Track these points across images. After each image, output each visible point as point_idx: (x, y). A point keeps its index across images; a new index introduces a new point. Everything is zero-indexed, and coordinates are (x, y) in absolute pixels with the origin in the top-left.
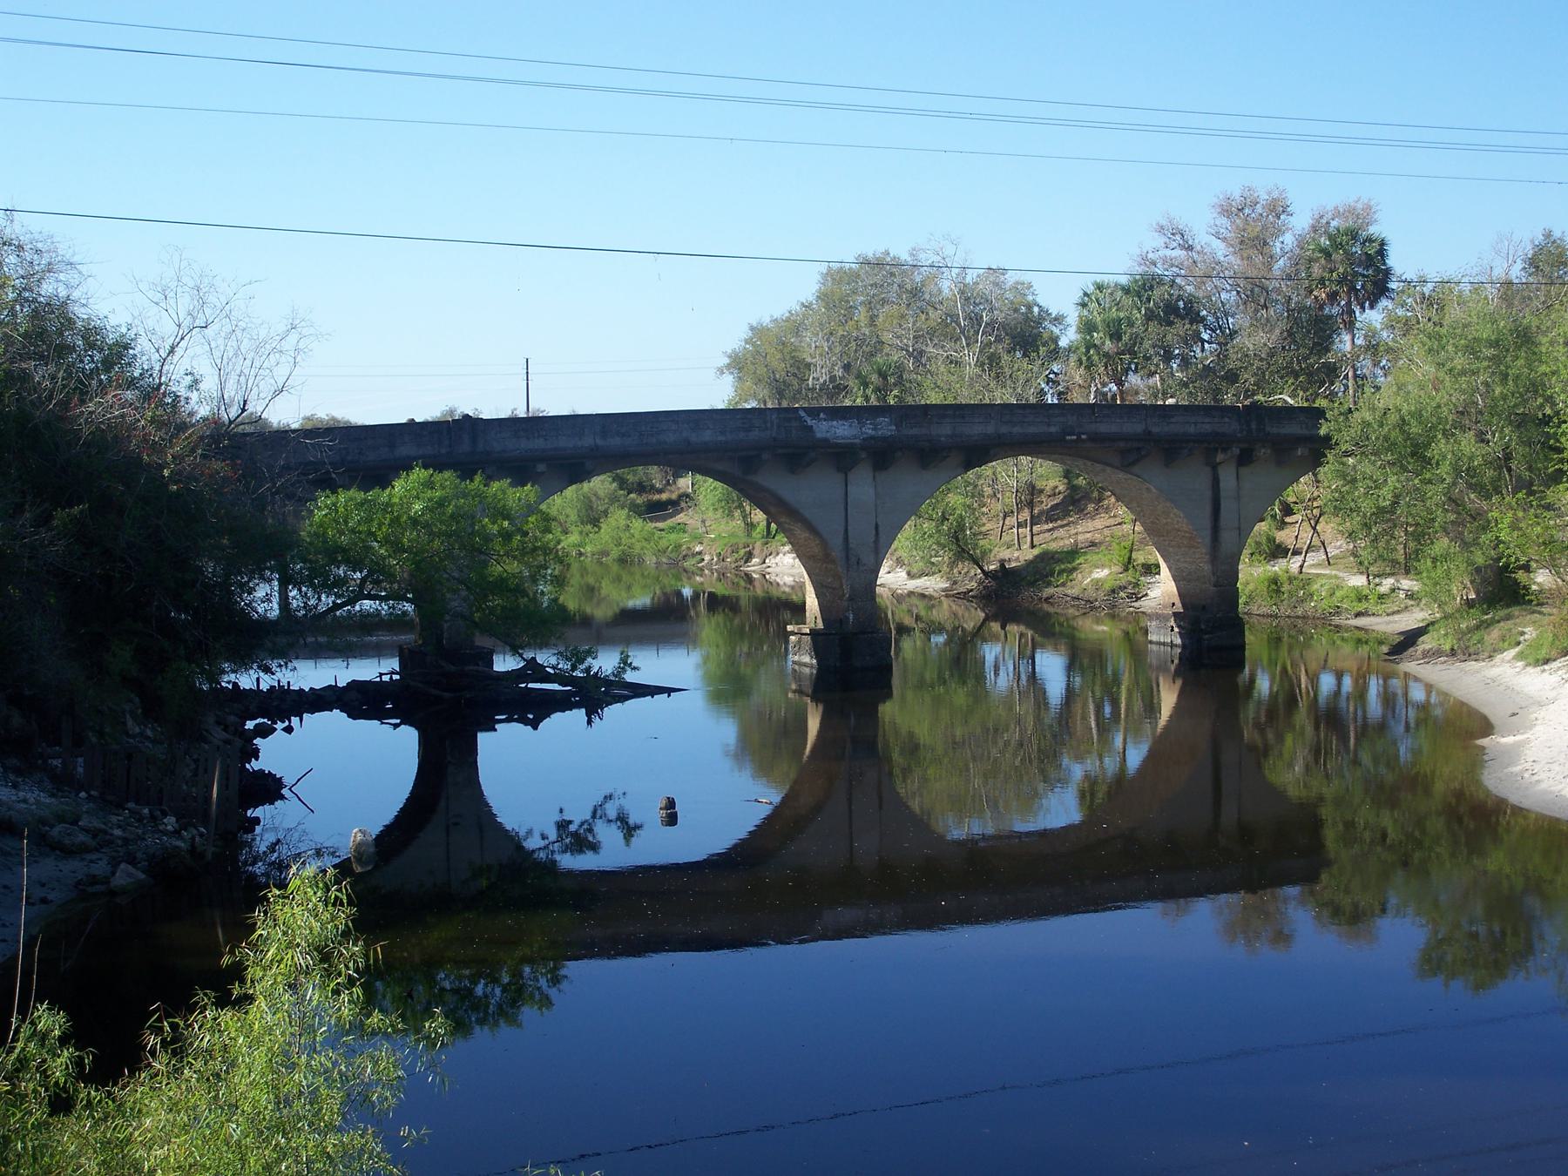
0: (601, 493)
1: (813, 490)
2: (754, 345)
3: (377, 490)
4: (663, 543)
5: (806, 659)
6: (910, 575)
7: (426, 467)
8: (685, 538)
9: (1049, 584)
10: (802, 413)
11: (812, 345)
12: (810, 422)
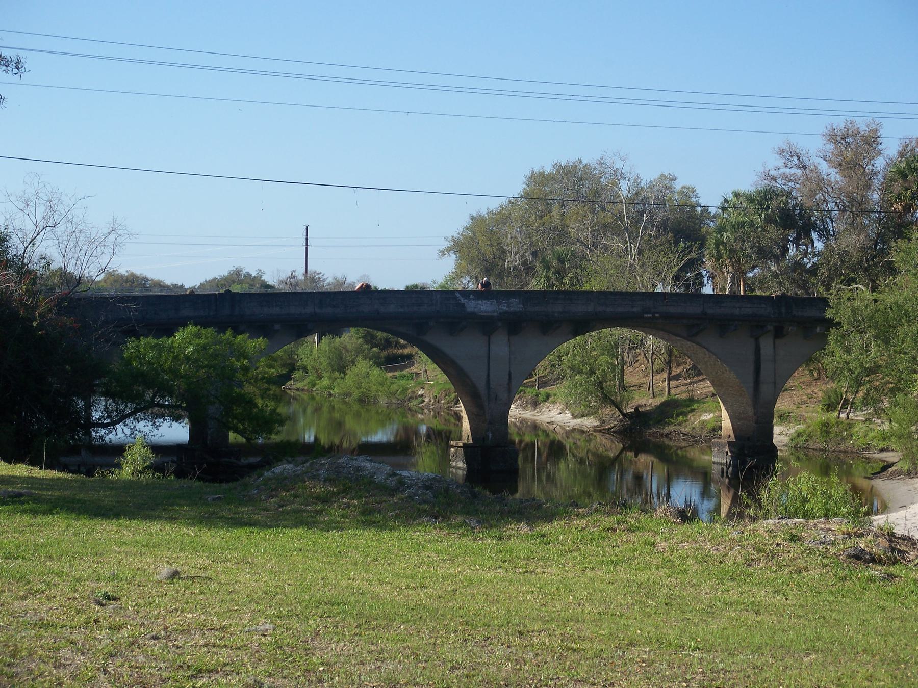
0: (349, 347)
1: (466, 348)
2: (474, 233)
3: (165, 338)
4: (394, 387)
5: (460, 464)
6: (574, 417)
7: (196, 325)
8: (411, 384)
9: (669, 424)
10: (458, 295)
11: (511, 235)
12: (463, 301)
